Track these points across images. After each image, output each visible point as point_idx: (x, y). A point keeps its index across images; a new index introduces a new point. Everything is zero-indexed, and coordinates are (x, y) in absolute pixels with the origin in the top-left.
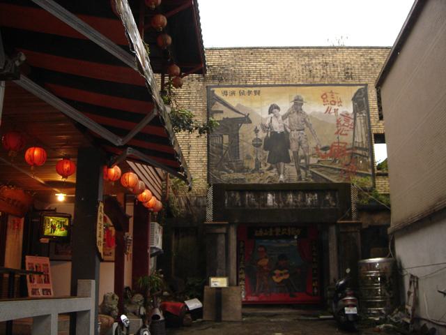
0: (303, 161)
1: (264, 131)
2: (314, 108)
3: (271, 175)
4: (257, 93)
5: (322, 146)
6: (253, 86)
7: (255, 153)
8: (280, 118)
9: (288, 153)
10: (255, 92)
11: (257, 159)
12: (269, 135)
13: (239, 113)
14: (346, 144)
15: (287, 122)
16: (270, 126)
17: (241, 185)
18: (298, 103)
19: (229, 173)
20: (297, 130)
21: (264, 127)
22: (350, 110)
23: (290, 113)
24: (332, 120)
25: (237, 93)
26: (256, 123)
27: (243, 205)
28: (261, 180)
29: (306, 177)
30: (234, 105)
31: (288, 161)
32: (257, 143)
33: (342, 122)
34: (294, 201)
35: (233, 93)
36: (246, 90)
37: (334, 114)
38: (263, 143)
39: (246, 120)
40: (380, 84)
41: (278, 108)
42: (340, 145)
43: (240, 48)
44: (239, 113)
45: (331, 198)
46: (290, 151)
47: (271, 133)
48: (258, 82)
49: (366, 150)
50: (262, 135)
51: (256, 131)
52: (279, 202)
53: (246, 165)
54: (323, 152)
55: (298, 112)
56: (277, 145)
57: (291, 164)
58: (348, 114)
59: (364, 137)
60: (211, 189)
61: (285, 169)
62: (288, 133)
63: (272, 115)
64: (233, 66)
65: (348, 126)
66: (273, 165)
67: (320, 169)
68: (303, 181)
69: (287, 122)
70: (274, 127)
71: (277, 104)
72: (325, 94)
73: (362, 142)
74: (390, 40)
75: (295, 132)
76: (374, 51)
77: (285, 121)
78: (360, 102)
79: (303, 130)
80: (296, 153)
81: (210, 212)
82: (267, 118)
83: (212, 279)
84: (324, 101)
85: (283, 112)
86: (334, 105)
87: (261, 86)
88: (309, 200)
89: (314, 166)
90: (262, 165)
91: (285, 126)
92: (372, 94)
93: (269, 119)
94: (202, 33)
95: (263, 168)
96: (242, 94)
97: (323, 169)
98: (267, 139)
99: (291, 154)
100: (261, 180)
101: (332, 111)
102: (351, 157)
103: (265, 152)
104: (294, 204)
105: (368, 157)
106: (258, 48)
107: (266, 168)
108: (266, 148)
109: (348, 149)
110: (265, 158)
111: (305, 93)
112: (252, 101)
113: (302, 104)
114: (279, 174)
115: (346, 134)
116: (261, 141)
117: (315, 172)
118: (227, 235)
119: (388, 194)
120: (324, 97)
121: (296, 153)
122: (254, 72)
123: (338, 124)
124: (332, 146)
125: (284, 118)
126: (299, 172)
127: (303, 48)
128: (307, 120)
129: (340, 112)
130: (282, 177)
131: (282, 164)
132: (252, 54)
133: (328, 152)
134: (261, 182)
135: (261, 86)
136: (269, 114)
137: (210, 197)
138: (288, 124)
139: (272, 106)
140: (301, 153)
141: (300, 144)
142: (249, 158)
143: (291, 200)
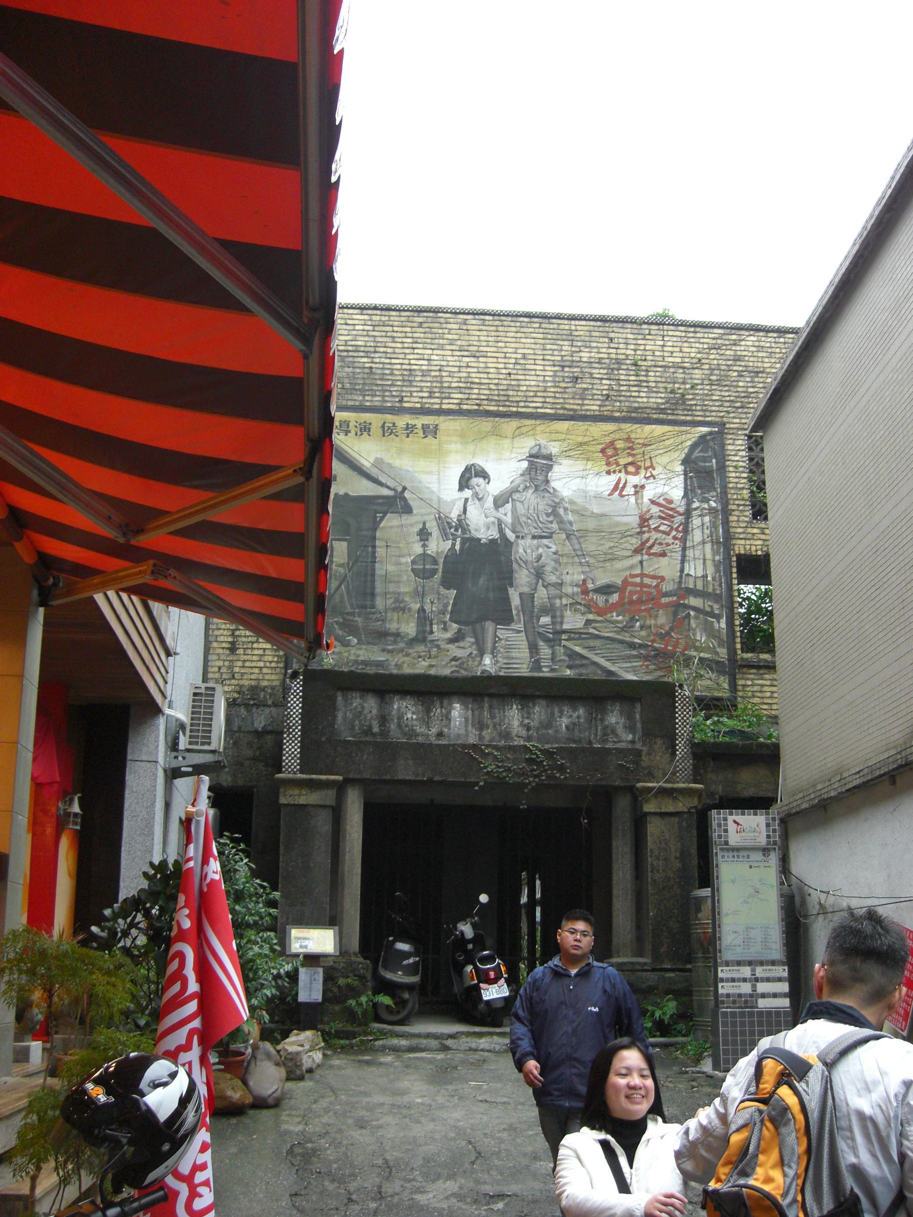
0: (545, 620)
1: (445, 536)
2: (578, 481)
3: (459, 653)
4: (431, 431)
5: (599, 583)
6: (424, 415)
7: (420, 594)
8: (489, 502)
9: (507, 600)
10: (425, 428)
11: (422, 610)
12: (457, 547)
13: (380, 484)
14: (662, 579)
15: (506, 514)
16: (462, 524)
17: (378, 676)
18: (539, 466)
19: (346, 644)
20: (534, 537)
21: (445, 525)
22: (676, 492)
23: (515, 490)
24: (626, 512)
25: (376, 428)
26: (422, 514)
27: (384, 733)
28: (431, 666)
29: (553, 666)
30: (366, 463)
31: (505, 618)
32: (423, 568)
33: (653, 523)
34: (522, 724)
35: (365, 429)
36: (402, 421)
37: (632, 499)
38: (440, 567)
39: (398, 503)
40: (767, 418)
41: (483, 474)
42: (647, 581)
43: (388, 309)
44: (380, 484)
45: (622, 721)
46: (511, 591)
47: (463, 543)
48: (435, 404)
49: (716, 598)
50: (438, 546)
51: (424, 535)
52: (481, 726)
53: (393, 627)
54: (600, 600)
55: (537, 488)
56: (478, 572)
57: (514, 626)
58: (671, 502)
59: (709, 563)
60: (297, 686)
61: (496, 639)
62: (508, 544)
63: (468, 493)
64: (367, 354)
65: (668, 534)
66: (466, 629)
67: (592, 643)
68: (546, 673)
69: (506, 514)
70: (472, 527)
71: (480, 461)
72: (612, 443)
73: (705, 576)
74: (799, 312)
75: (528, 541)
76: (751, 339)
77: (501, 510)
78: (702, 472)
79: (549, 537)
80: (528, 599)
81: (292, 750)
82: (453, 502)
83: (295, 933)
84: (608, 464)
85: (497, 485)
86: (636, 473)
87: (440, 412)
88: (564, 722)
89: (576, 635)
90: (435, 627)
91: (500, 522)
92: (737, 450)
93: (459, 506)
94: (336, 221)
95: (438, 633)
96: (388, 431)
97: (597, 643)
98: (451, 558)
99: (515, 601)
100: (431, 666)
101: (629, 490)
102: (675, 614)
103: (443, 591)
104: (524, 733)
105: (718, 617)
106: (436, 311)
107: (449, 635)
108: (447, 583)
109: (666, 594)
110: (446, 605)
111: (549, 438)
112: (400, 451)
113: (550, 468)
114: (482, 653)
115: (663, 554)
116: (435, 561)
117: (578, 649)
118: (337, 814)
119: (776, 717)
120: (610, 452)
121: (528, 599)
122: (425, 373)
123: (641, 526)
124: (625, 582)
125: (499, 502)
126: (533, 648)
127: (558, 317)
128: (561, 511)
129: (649, 493)
130: (487, 660)
131: (490, 626)
132: (420, 325)
133: (615, 598)
134: (432, 672)
135: (440, 412)
136: (461, 489)
137: (295, 706)
138: (508, 519)
139: (468, 469)
140: (542, 594)
141: (539, 574)
142: (400, 608)
143: (516, 723)
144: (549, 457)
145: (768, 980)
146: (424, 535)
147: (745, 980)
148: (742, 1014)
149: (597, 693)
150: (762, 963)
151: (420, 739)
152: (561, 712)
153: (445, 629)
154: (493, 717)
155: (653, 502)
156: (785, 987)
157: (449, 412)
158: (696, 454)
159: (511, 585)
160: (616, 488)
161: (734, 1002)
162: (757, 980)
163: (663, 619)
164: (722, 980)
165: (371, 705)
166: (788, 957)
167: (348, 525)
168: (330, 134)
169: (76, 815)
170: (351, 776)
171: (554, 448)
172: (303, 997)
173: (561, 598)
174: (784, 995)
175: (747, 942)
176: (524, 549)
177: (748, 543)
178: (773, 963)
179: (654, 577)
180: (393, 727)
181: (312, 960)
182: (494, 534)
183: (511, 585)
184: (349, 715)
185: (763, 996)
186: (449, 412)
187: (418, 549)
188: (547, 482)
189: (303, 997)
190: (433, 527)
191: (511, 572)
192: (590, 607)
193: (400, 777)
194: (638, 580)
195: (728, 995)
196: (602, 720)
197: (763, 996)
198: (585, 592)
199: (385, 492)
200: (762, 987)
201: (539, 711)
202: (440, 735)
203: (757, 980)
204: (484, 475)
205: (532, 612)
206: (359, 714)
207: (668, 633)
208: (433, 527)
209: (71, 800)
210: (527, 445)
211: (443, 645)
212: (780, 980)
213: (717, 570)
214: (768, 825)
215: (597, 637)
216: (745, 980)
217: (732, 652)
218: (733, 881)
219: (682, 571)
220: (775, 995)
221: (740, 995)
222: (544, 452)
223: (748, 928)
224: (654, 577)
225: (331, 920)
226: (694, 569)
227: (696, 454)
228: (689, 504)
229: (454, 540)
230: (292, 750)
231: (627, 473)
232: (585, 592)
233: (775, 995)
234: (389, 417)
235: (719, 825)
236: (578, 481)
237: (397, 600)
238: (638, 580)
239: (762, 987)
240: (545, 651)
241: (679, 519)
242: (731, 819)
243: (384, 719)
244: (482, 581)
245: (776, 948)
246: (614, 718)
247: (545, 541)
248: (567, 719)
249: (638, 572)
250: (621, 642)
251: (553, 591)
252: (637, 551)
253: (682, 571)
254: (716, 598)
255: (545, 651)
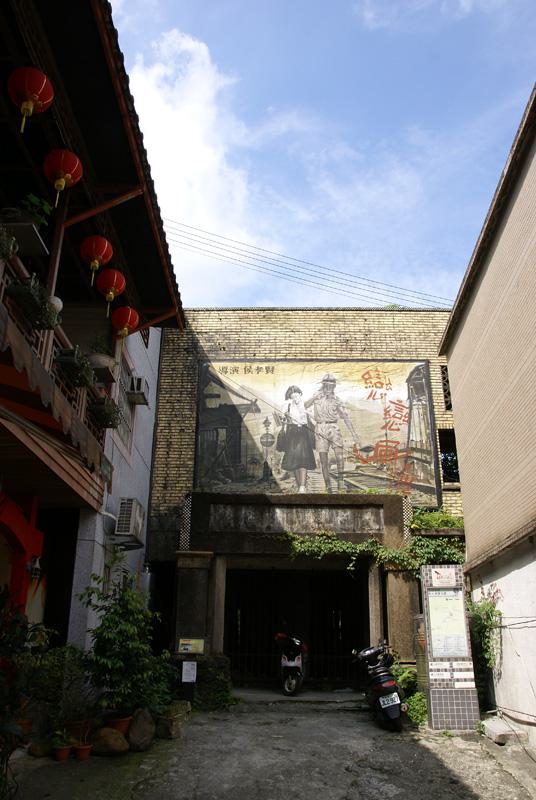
0: (334, 466)
1: (278, 424)
5: (364, 446)
8: (302, 406)
14: (398, 443)
15: (311, 411)
18: (328, 385)
21: (278, 418)
26: (267, 412)
29: (338, 488)
31: (312, 465)
33: (392, 413)
35: (236, 370)
36: (255, 366)
38: (276, 440)
42: (389, 444)
45: (373, 518)
46: (314, 451)
47: (288, 427)
48: (272, 356)
50: (275, 429)
51: (267, 423)
58: (401, 402)
59: (424, 434)
61: (307, 478)
63: (290, 401)
66: (291, 473)
67: (360, 478)
69: (311, 411)
72: (368, 373)
75: (324, 424)
78: (419, 384)
79: (335, 422)
80: (324, 455)
81: (185, 537)
85: (307, 396)
88: (339, 519)
89: (351, 474)
96: (247, 370)
98: (282, 436)
99: (317, 457)
101: (378, 396)
102: (406, 461)
105: (430, 463)
107: (281, 476)
108: (279, 448)
109: (400, 451)
110: (279, 461)
111: (334, 370)
113: (334, 386)
114: (299, 485)
115: (399, 430)
116: (273, 437)
117: (352, 482)
118: (210, 573)
121: (324, 455)
123: (385, 414)
125: (307, 406)
126: (327, 482)
131: (303, 471)
133: (372, 454)
136: (286, 399)
137: (187, 513)
138: (312, 414)
139: (290, 389)
140: (331, 454)
141: (330, 442)
144: (334, 381)
145: (461, 670)
146: (267, 423)
147: (446, 670)
148: (445, 692)
149: (356, 504)
150: (456, 659)
151: (258, 530)
152: (337, 513)
153: (279, 473)
154: (298, 517)
155: (391, 402)
156: (471, 675)
157: (278, 360)
158: (413, 377)
159: (315, 448)
160: (370, 396)
161: (440, 684)
162: (453, 670)
163: (399, 465)
164: (431, 670)
165: (229, 512)
166: (473, 655)
167: (226, 420)
168: (148, 168)
169: (37, 569)
170: (219, 551)
171: (336, 376)
172: (185, 679)
173: (342, 454)
174: (471, 680)
175: (446, 647)
176: (322, 429)
177: (444, 421)
178: (463, 659)
179: (393, 442)
180: (242, 524)
181: (191, 657)
182: (305, 422)
183: (315, 448)
184: (218, 518)
185: (458, 680)
186: (278, 360)
187: (263, 431)
188: (333, 393)
189: (185, 679)
190: (272, 419)
191: (315, 441)
192: (359, 458)
193: (246, 552)
194: (384, 444)
195: (436, 680)
196: (361, 518)
197: (458, 680)
198: (356, 451)
199: (246, 402)
200: (457, 675)
201: (325, 513)
202: (269, 528)
203: (453, 670)
204: (299, 391)
205: (326, 462)
206: (223, 516)
207: (402, 472)
208: (272, 419)
209: (35, 561)
210: (322, 375)
211: (279, 482)
212: (468, 670)
213: (428, 438)
214: (456, 574)
215: (363, 475)
216: (446, 670)
217: (438, 483)
218: (436, 609)
219: (409, 438)
220: (465, 680)
221: (443, 680)
222: (331, 378)
223: (447, 638)
224: (393, 442)
225: (204, 632)
226: (416, 437)
227: (413, 377)
228: (411, 403)
229: (283, 425)
230: (185, 537)
231: (377, 387)
232: (356, 451)
233: (465, 680)
234: (248, 364)
235: (427, 574)
236: (351, 391)
237: (253, 458)
238: (384, 444)
239: (457, 675)
240: (334, 483)
241: (406, 411)
242: (433, 570)
243: (237, 519)
244: (299, 446)
245: (465, 649)
246: (368, 516)
247: (333, 425)
248: (342, 516)
249: (384, 439)
250: (377, 478)
251: (338, 450)
252: (384, 428)
253: (409, 438)
254: (428, 453)
255: (334, 483)
